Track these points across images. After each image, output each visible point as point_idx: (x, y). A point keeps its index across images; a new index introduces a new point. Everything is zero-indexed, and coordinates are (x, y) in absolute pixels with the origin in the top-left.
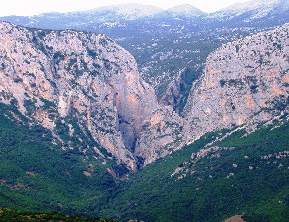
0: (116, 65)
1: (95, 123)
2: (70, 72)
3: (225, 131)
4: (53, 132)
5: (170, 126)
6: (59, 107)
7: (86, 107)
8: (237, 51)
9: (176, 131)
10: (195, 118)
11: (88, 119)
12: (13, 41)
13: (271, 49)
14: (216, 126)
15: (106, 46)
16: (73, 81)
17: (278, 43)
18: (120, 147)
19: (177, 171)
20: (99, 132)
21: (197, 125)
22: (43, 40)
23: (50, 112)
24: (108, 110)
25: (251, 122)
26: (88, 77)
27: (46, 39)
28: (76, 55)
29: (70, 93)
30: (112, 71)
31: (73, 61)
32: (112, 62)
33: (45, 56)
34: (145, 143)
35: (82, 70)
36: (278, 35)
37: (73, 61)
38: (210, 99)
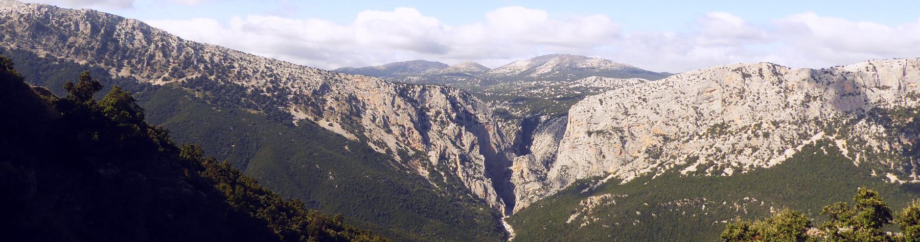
12: (382, 95)
16: (440, 132)
19: (572, 217)
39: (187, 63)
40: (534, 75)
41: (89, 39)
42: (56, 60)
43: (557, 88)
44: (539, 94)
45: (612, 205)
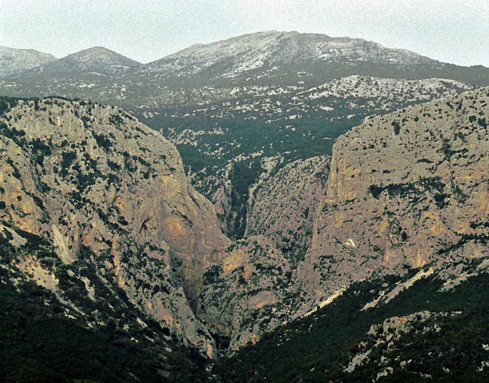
0: (143, 162)
1: (131, 274)
2: (68, 177)
3: (393, 280)
4: (57, 295)
5: (267, 272)
6: (55, 244)
7: (109, 243)
8: (397, 132)
9: (280, 281)
10: (324, 257)
11: (114, 267)
13: (467, 128)
14: (372, 271)
15: (122, 126)
16: (75, 196)
17: (478, 117)
18: (184, 316)
19: (358, 360)
20: (140, 289)
21: (331, 270)
22: (6, 117)
23: (43, 257)
24: (151, 247)
25: (447, 260)
26: (107, 188)
27: (11, 117)
28: (73, 146)
30: (138, 175)
31: (69, 158)
32: (135, 158)
33: (19, 150)
34: (216, 305)
35: (90, 174)
36: (474, 102)
37: (69, 158)
38: (351, 221)
40: (231, 75)
43: (285, 100)
44: (252, 113)
45: (431, 335)
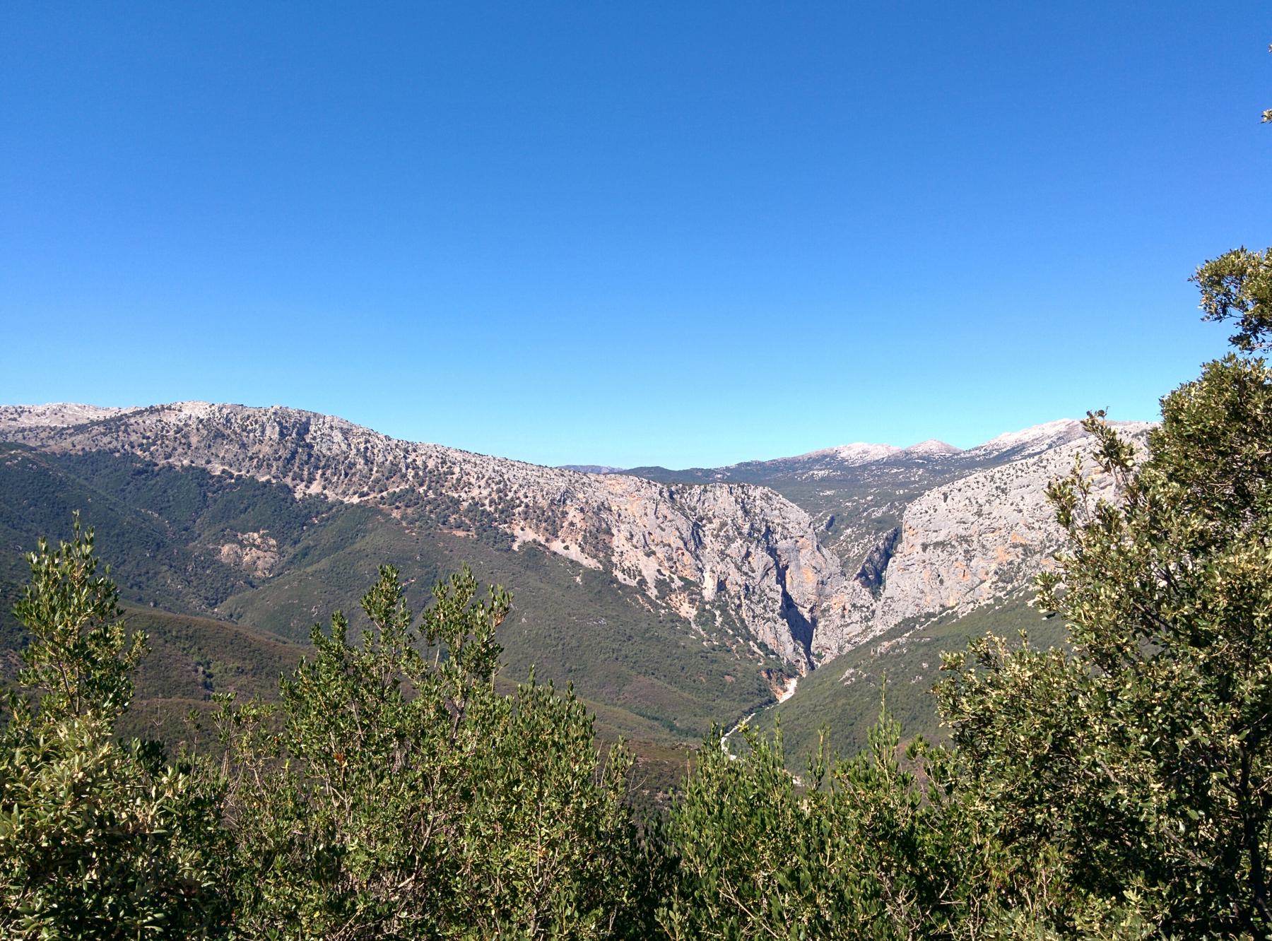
16: (722, 552)
29: (719, 567)
31: (724, 525)
39: (394, 470)
41: (276, 447)
42: (231, 477)
